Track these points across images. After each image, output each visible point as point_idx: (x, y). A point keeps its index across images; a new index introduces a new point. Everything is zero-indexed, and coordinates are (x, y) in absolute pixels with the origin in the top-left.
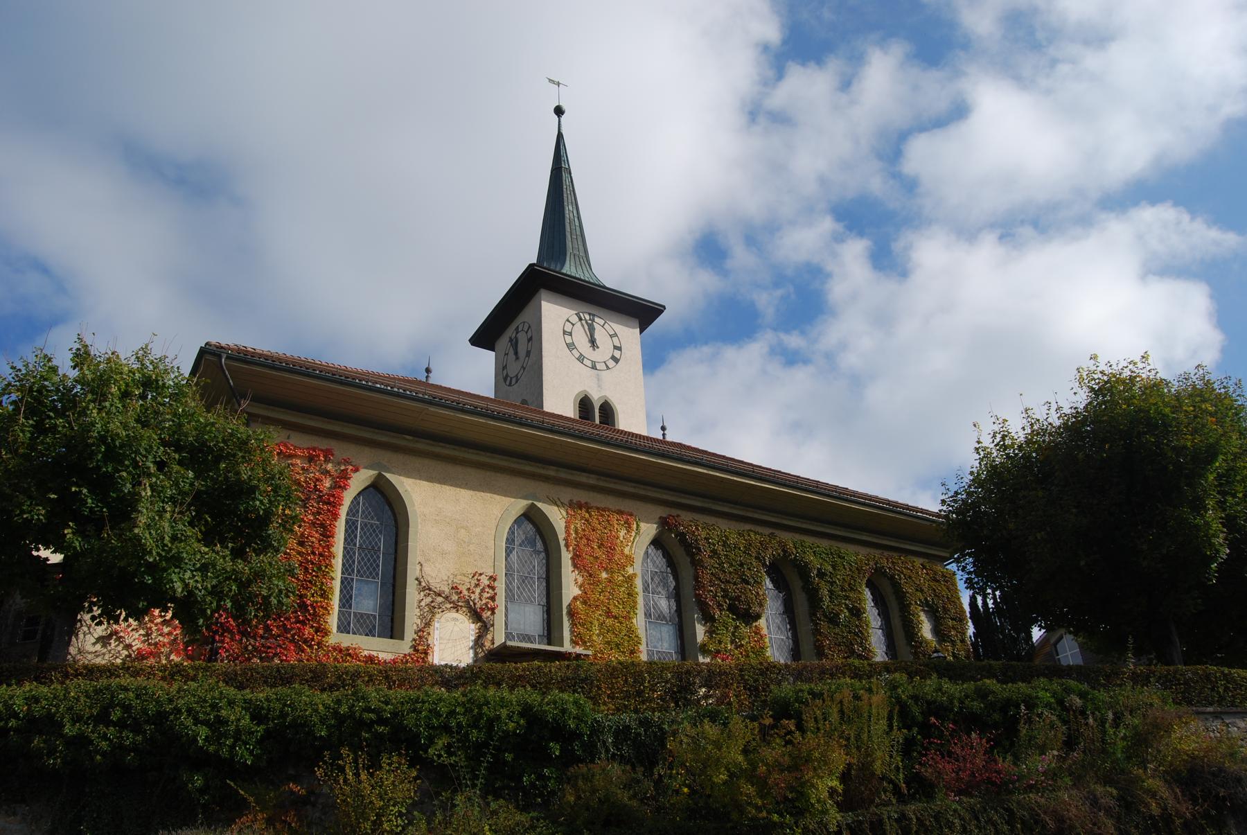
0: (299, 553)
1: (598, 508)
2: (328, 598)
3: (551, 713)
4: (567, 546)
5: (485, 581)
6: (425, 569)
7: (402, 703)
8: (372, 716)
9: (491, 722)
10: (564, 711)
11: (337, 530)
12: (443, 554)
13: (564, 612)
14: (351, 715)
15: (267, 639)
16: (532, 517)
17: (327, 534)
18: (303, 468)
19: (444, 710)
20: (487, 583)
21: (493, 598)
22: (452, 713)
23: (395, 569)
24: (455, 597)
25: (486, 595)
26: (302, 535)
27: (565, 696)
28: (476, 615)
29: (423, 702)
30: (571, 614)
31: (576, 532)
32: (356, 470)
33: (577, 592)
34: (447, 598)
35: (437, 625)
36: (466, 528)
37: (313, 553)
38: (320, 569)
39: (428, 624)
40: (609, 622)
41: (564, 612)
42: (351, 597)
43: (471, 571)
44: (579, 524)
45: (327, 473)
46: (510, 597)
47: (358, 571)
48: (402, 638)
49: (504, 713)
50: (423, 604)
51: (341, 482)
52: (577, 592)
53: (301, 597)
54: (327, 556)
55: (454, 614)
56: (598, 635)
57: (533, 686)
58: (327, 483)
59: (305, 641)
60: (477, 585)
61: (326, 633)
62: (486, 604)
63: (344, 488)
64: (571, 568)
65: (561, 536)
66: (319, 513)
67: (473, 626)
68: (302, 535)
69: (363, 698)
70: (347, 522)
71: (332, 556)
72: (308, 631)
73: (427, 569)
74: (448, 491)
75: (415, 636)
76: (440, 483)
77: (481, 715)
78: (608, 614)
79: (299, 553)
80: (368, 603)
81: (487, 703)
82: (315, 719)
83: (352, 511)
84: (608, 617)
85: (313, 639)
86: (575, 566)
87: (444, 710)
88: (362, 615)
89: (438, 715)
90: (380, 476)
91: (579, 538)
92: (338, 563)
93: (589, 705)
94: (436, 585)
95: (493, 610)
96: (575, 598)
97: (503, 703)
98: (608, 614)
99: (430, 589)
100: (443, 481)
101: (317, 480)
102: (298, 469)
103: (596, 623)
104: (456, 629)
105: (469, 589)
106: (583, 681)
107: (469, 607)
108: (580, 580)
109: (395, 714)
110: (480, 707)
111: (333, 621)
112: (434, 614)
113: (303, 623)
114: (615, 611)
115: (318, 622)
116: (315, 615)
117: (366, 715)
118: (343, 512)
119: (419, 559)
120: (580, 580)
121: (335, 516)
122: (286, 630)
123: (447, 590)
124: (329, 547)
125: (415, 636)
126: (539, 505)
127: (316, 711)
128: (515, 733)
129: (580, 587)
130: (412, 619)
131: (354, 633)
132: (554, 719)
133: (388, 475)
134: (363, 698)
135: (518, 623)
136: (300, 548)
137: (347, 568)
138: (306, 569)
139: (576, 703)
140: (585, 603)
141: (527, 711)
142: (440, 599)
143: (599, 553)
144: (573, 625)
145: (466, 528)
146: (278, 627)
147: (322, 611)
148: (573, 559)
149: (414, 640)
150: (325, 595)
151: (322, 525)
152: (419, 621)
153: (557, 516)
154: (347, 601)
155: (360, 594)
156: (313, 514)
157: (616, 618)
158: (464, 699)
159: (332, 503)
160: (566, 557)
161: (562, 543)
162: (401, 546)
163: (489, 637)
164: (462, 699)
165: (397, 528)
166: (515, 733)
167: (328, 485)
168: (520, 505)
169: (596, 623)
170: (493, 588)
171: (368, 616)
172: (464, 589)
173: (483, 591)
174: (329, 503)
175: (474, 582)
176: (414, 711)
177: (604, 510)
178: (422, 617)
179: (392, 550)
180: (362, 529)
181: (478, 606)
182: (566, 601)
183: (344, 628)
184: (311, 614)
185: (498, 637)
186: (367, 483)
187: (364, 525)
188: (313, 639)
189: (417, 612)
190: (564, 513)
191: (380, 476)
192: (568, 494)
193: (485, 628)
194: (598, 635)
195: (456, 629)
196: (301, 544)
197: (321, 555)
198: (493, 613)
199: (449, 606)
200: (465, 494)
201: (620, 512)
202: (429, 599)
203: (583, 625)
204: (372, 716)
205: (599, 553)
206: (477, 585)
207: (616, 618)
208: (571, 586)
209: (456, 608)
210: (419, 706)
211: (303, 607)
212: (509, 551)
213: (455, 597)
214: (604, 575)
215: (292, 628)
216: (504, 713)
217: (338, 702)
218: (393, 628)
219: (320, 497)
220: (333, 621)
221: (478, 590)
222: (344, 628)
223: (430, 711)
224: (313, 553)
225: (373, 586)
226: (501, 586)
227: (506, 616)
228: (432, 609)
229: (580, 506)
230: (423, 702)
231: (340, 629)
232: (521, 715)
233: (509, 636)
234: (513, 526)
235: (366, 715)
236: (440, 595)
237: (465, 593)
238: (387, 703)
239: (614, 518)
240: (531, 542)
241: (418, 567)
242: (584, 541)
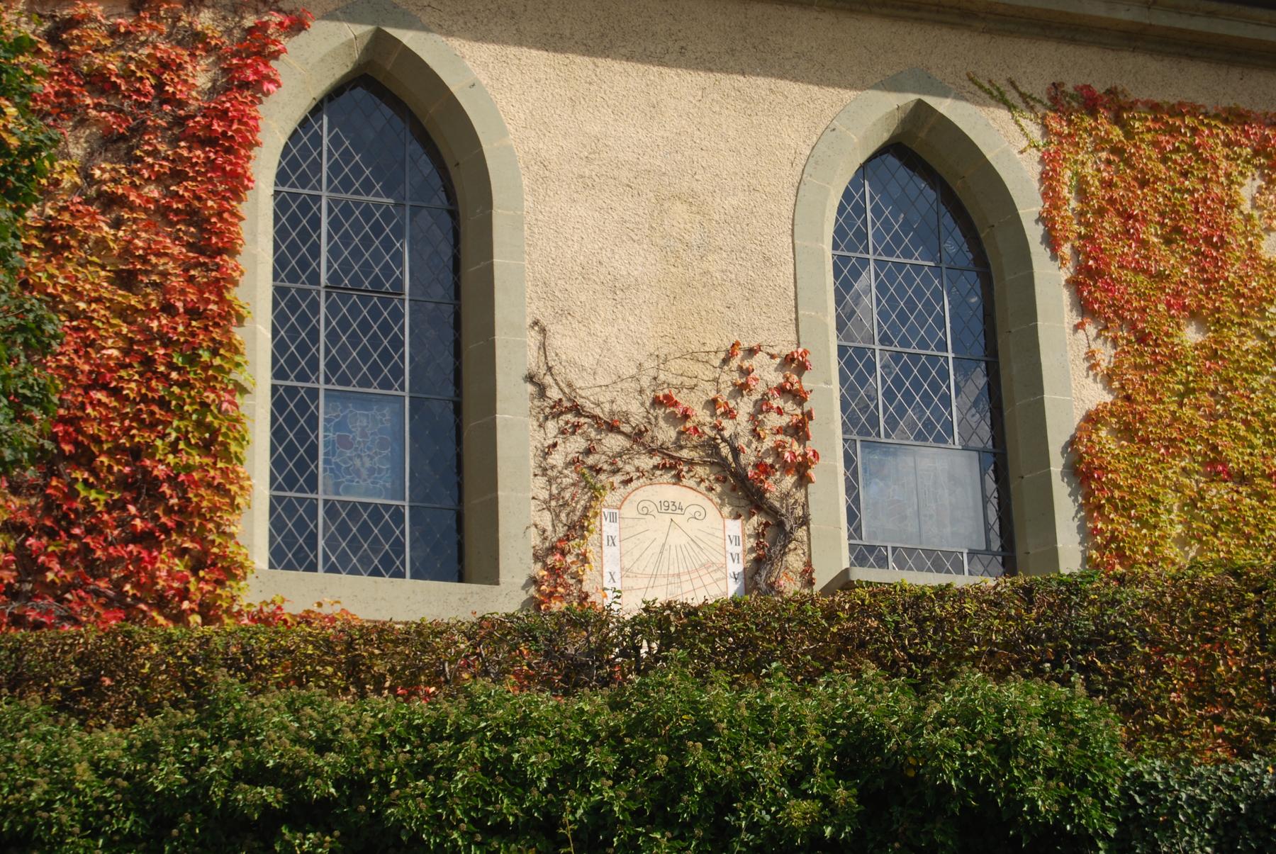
0: (124, 313)
1: (1154, 107)
2: (227, 455)
3: (952, 756)
4: (1052, 241)
5: (767, 374)
6: (555, 342)
7: (382, 744)
8: (269, 794)
9: (723, 798)
10: (1005, 748)
11: (244, 228)
12: (617, 289)
13: (1057, 465)
14: (196, 795)
15: (31, 596)
16: (922, 163)
17: (212, 245)
18: (113, 32)
19: (538, 761)
20: (776, 379)
21: (799, 430)
22: (571, 773)
23: (458, 354)
24: (666, 434)
25: (773, 421)
26: (127, 251)
27: (1012, 692)
28: (743, 490)
29: (460, 736)
30: (1083, 472)
31: (1082, 191)
32: (297, 25)
33: (1095, 395)
34: (637, 435)
35: (609, 528)
36: (690, 199)
37: (168, 309)
38: (193, 359)
39: (578, 528)
40: (1219, 493)
41: (1057, 465)
42: (313, 452)
43: (718, 341)
44: (1091, 165)
45: (195, 41)
46: (858, 420)
47: (332, 365)
48: (491, 576)
49: (770, 763)
50: (557, 459)
51: (247, 69)
52: (1095, 395)
53: (136, 453)
54: (214, 315)
55: (664, 490)
56: (1182, 542)
57: (891, 669)
58: (201, 75)
59: (161, 602)
60: (741, 389)
61: (229, 571)
62: (777, 451)
63: (258, 86)
64: (1070, 317)
65: (1029, 206)
66: (178, 176)
67: (735, 527)
68: (127, 251)
69: (238, 733)
70: (281, 204)
71: (231, 315)
72: (167, 567)
73: (564, 342)
74: (622, 80)
75: (538, 570)
76: (588, 51)
77: (680, 777)
78: (1215, 467)
79: (124, 313)
80: (369, 458)
81: (704, 730)
82: (61, 814)
83: (295, 164)
84: (1213, 477)
85: (184, 594)
86: (1085, 308)
87: (538, 761)
88: (354, 510)
89: (518, 780)
90: (380, 42)
91: (1092, 212)
92: (256, 337)
93: (1110, 729)
94: (598, 394)
95: (802, 471)
96: (1093, 419)
97: (765, 728)
98: (1215, 467)
99: (577, 410)
100: (760, 85)
101: (165, 65)
102: (96, 35)
103: (1171, 499)
104: (677, 538)
105: (713, 403)
106: (1089, 643)
107: (720, 464)
108: (1106, 355)
109: (354, 785)
110: (677, 750)
111: (251, 531)
112: (595, 493)
113: (147, 539)
114: (1236, 457)
115: (200, 538)
116: (185, 510)
117: (246, 795)
118: (263, 168)
119: (534, 309)
120: (1106, 355)
121: (237, 184)
122: (93, 568)
123: (636, 410)
124: (220, 285)
125: (538, 570)
126: (944, 106)
127: (67, 786)
128: (815, 838)
129: (1108, 378)
130: (522, 514)
131: (332, 569)
132: (969, 781)
133: (407, 37)
134: (238, 733)
135: (886, 517)
136: (121, 296)
137: (290, 356)
138: (148, 362)
139: (1052, 717)
140: (1126, 432)
141: (856, 751)
142: (614, 442)
143: (1167, 259)
144: (1090, 508)
145: (690, 199)
146: (64, 559)
147: (207, 499)
148: (1074, 285)
149: (534, 581)
150: (215, 442)
151: (193, 216)
152: (546, 519)
153: (1009, 143)
154: (302, 466)
155: (345, 443)
156: (159, 179)
157: (1242, 479)
158: (619, 719)
159: (224, 141)
160: (1051, 280)
161: (1034, 233)
162: (470, 270)
163: (795, 561)
164: (608, 719)
165: (454, 214)
166: (815, 838)
167: (203, 80)
168: (871, 115)
169: (1171, 499)
170: (799, 397)
171: (376, 512)
172: (694, 403)
173: (762, 406)
174: (209, 141)
175: (729, 378)
176: (423, 769)
177: (1177, 111)
178: (555, 503)
179: (440, 292)
180: (335, 224)
181: (749, 457)
182: (1061, 423)
183: (292, 550)
184: (179, 514)
185: (826, 552)
186: (339, 70)
187: (342, 213)
188: (184, 594)
189: (539, 487)
190: (1035, 132)
191: (380, 42)
192: (1043, 64)
193: (776, 531)
194: (1182, 542)
195: (677, 538)
196: (126, 280)
197: (192, 312)
198: (804, 480)
199: (646, 462)
200: (680, 87)
201: (1236, 117)
202: (576, 444)
203: (1125, 508)
204: (269, 794)
205: (1167, 259)
206: (741, 389)
207: (1242, 479)
208: (1073, 376)
209: (673, 467)
210: (442, 749)
211: (142, 487)
212: (846, 273)
213: (666, 434)
214: (1191, 335)
215: (112, 562)
216: (770, 763)
217: (149, 751)
218: (454, 536)
219: (179, 121)
220: (251, 531)
221: (744, 407)
222: (292, 550)
223: (487, 768)
224: (168, 309)
225: (385, 414)
226: (825, 388)
227: (851, 488)
228: (591, 476)
229: (1090, 103)
230: (460, 736)
231: (278, 558)
232: (841, 772)
233: (862, 555)
234: (856, 183)
235: (246, 795)
236: (612, 428)
237: (701, 415)
238: (322, 747)
239: (1215, 140)
240: (930, 241)
241: (533, 338)
242: (1112, 223)
